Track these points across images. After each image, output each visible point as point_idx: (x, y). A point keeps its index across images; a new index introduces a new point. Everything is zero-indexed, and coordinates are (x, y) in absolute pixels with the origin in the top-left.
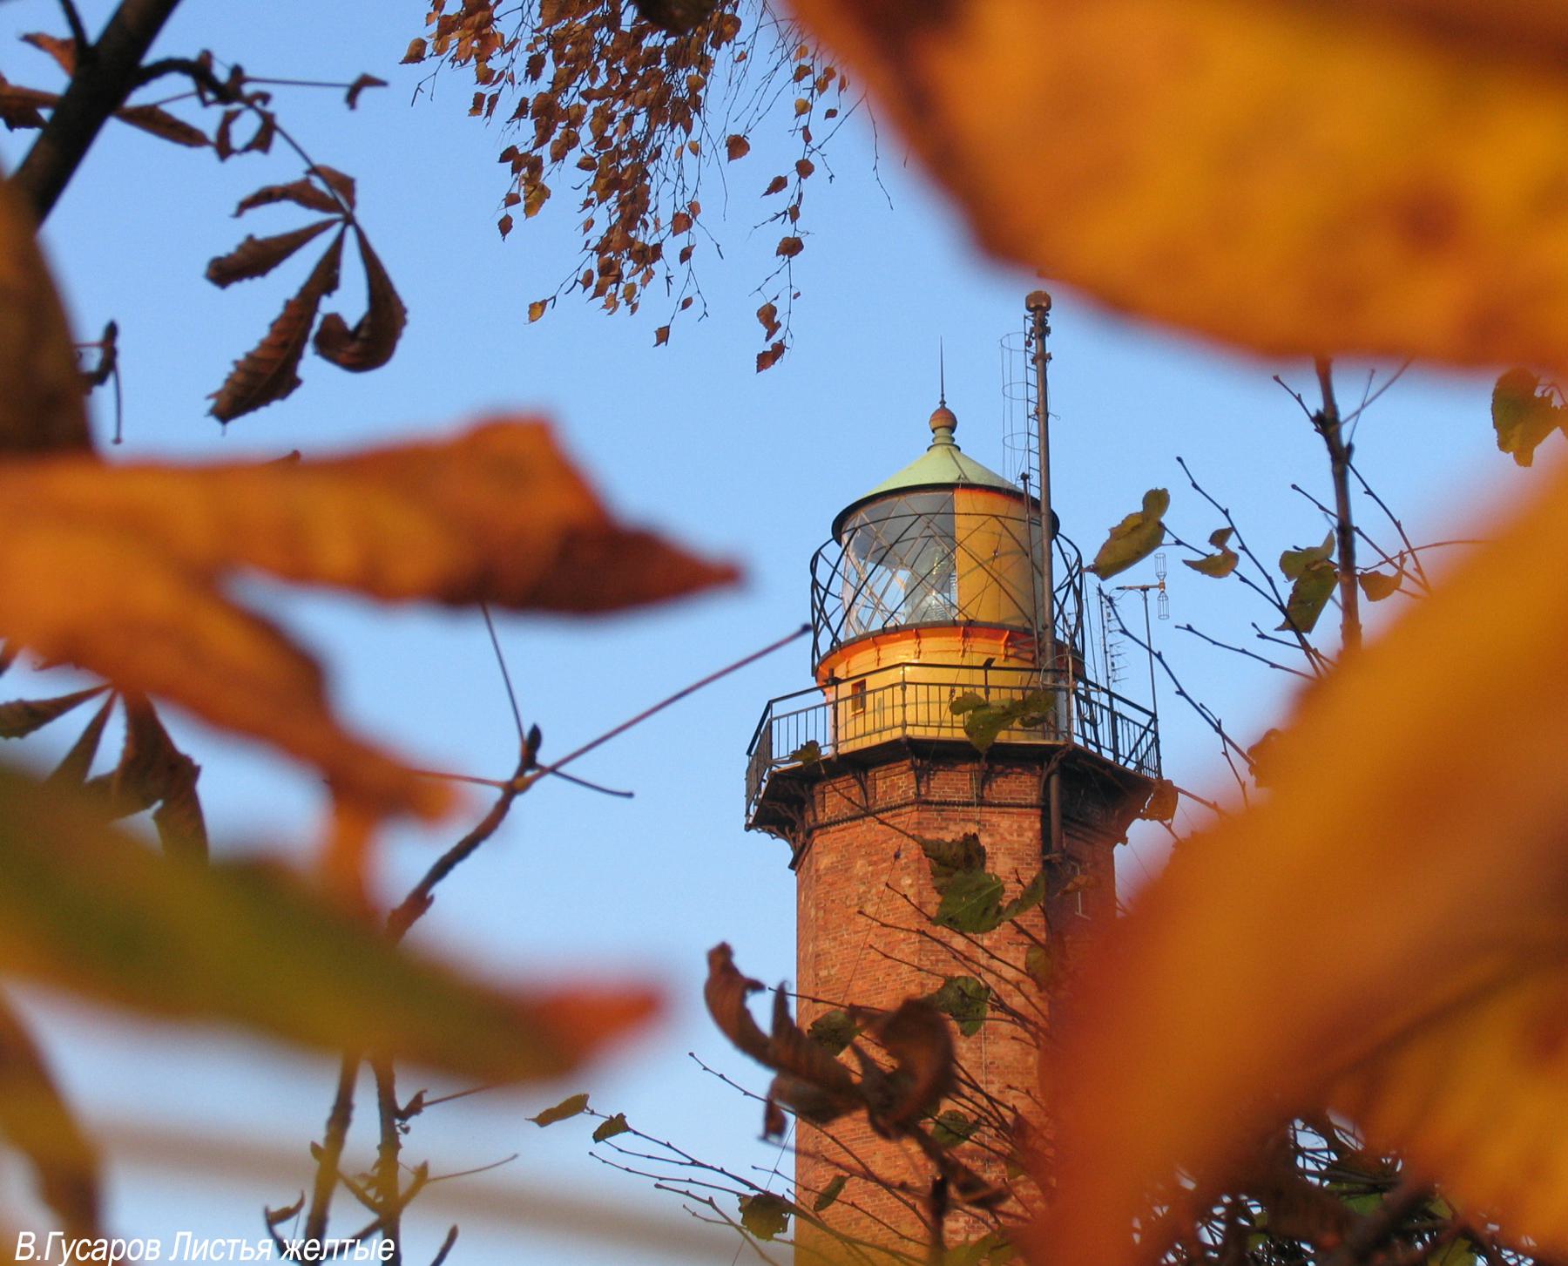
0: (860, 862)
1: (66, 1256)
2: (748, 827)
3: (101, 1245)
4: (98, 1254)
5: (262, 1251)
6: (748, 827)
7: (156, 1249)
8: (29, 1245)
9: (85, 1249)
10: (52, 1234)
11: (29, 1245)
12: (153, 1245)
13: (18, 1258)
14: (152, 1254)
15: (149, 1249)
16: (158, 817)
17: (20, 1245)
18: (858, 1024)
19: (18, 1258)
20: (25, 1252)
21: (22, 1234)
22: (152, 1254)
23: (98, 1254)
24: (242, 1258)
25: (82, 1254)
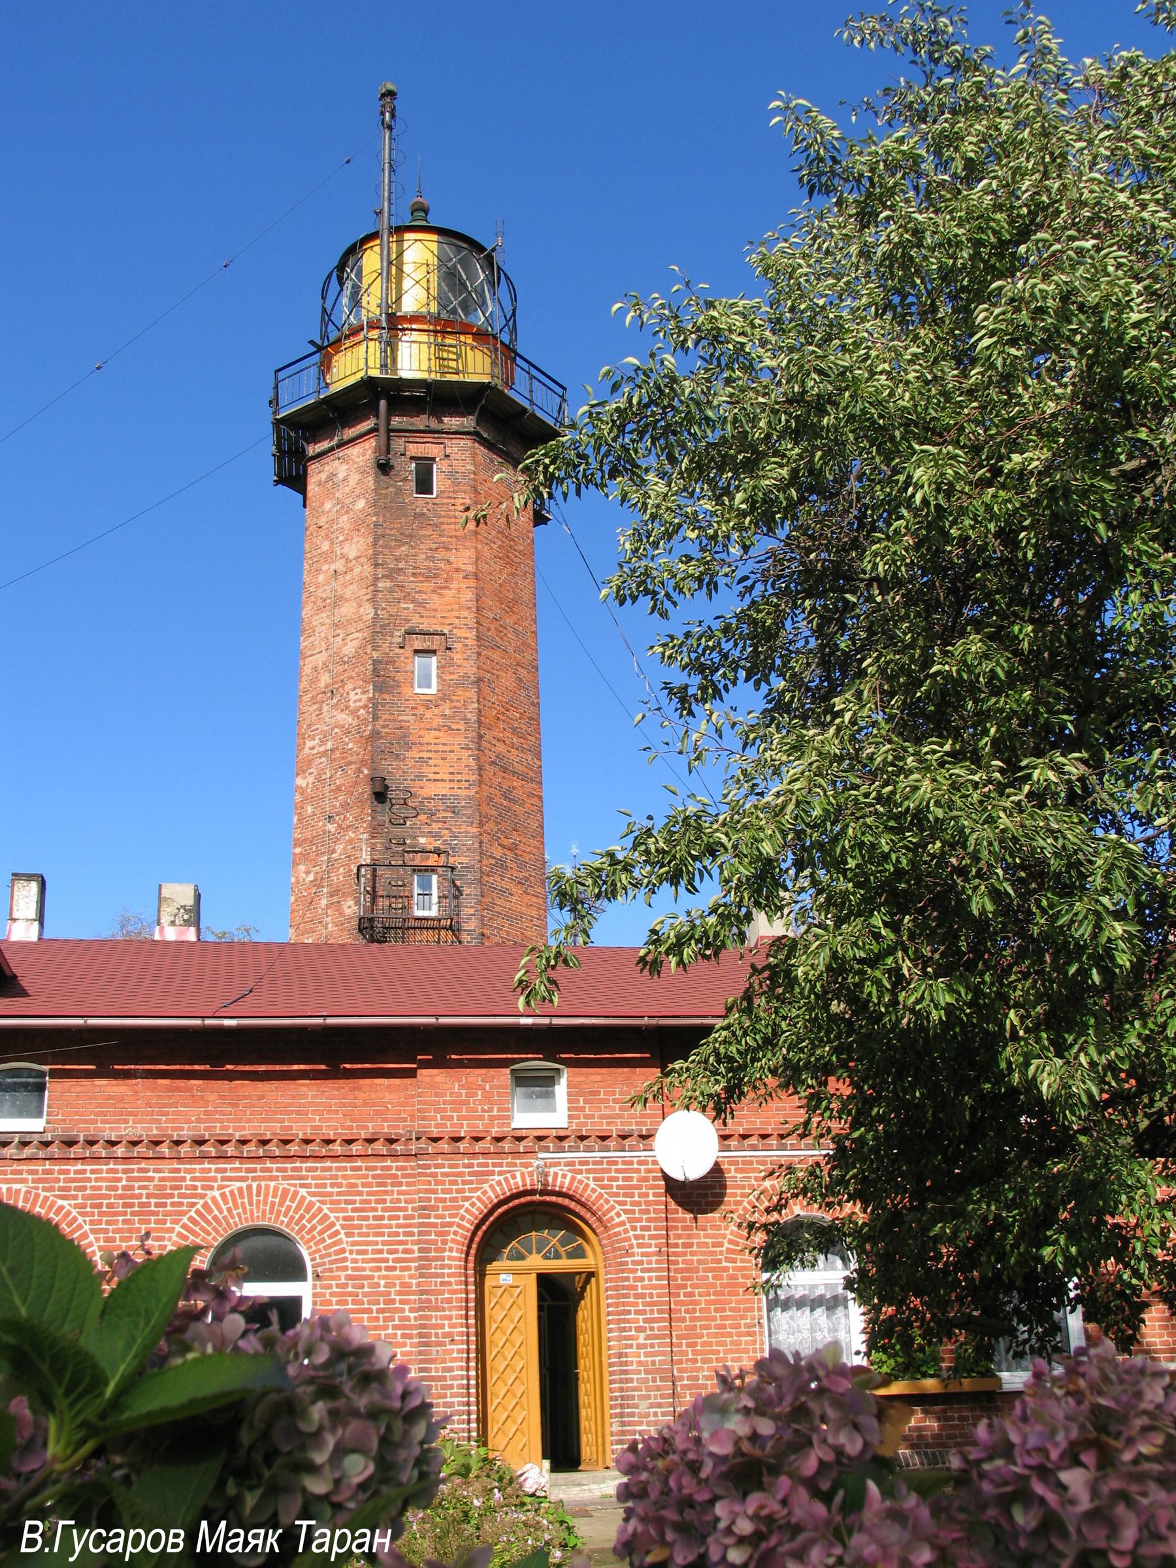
0: (1055, 1373)
1: (78, 1549)
2: (277, 482)
3: (117, 1535)
4: (114, 1546)
5: (253, 1542)
6: (277, 482)
7: (180, 1540)
8: (36, 1536)
9: (100, 1540)
10: (61, 1523)
11: (36, 1536)
12: (177, 1536)
13: (23, 1550)
14: (175, 1545)
15: (171, 1540)
16: (793, 1390)
17: (26, 1535)
18: (834, 1058)
19: (23, 1550)
20: (31, 1543)
21: (28, 1523)
22: (175, 1545)
23: (114, 1546)
24: (169, 1550)
25: (96, 1546)
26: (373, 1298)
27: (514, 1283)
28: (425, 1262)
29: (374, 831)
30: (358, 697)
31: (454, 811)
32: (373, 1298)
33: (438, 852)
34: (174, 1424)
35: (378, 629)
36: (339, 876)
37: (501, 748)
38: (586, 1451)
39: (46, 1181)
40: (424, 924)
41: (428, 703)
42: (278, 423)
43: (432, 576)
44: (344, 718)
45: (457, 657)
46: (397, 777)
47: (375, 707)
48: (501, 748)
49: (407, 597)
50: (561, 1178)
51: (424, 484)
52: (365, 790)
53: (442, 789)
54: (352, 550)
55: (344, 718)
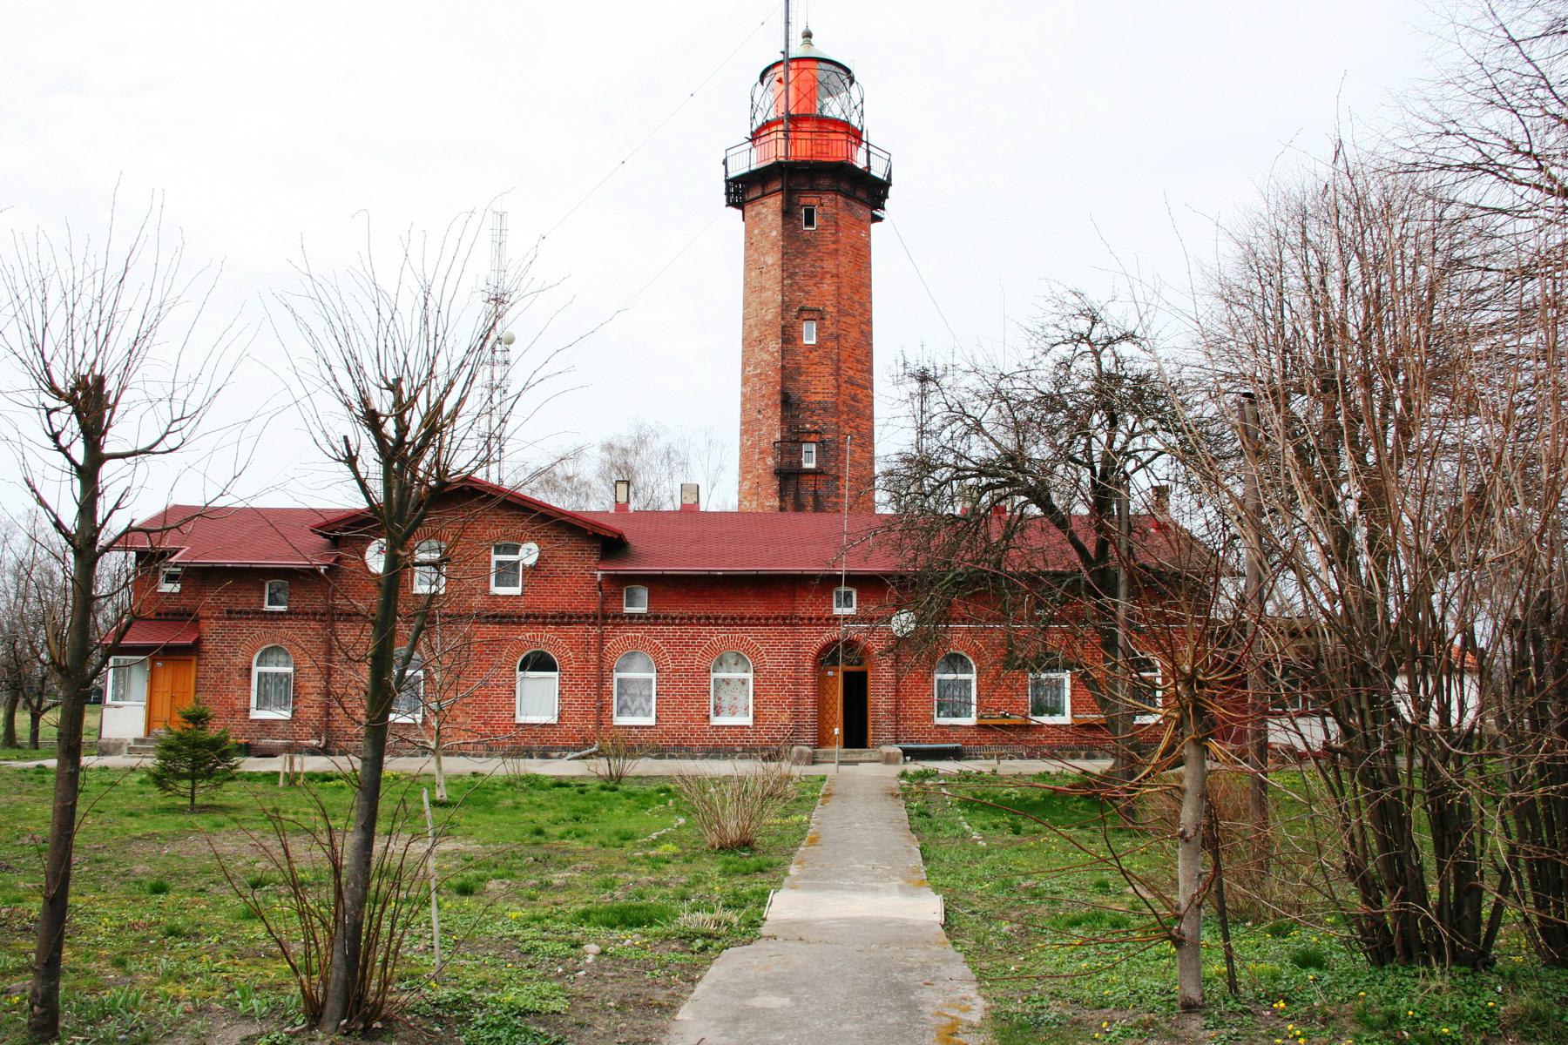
26: (777, 680)
27: (836, 676)
28: (797, 667)
29: (783, 420)
30: (775, 346)
31: (825, 409)
32: (777, 680)
33: (816, 432)
34: (356, 516)
35: (785, 307)
36: (764, 444)
37: (851, 373)
38: (870, 740)
39: (649, 633)
40: (809, 472)
41: (811, 349)
42: (727, 181)
43: (812, 276)
44: (766, 356)
45: (827, 323)
46: (795, 395)
47: (783, 352)
48: (851, 373)
49: (800, 289)
50: (853, 634)
51: (810, 222)
52: (778, 398)
53: (819, 398)
54: (770, 260)
55: (766, 356)
